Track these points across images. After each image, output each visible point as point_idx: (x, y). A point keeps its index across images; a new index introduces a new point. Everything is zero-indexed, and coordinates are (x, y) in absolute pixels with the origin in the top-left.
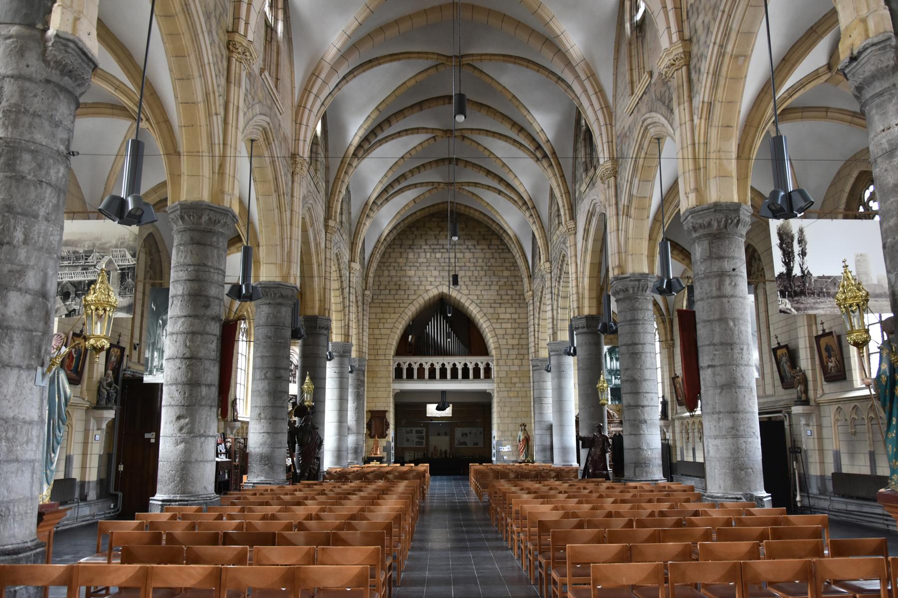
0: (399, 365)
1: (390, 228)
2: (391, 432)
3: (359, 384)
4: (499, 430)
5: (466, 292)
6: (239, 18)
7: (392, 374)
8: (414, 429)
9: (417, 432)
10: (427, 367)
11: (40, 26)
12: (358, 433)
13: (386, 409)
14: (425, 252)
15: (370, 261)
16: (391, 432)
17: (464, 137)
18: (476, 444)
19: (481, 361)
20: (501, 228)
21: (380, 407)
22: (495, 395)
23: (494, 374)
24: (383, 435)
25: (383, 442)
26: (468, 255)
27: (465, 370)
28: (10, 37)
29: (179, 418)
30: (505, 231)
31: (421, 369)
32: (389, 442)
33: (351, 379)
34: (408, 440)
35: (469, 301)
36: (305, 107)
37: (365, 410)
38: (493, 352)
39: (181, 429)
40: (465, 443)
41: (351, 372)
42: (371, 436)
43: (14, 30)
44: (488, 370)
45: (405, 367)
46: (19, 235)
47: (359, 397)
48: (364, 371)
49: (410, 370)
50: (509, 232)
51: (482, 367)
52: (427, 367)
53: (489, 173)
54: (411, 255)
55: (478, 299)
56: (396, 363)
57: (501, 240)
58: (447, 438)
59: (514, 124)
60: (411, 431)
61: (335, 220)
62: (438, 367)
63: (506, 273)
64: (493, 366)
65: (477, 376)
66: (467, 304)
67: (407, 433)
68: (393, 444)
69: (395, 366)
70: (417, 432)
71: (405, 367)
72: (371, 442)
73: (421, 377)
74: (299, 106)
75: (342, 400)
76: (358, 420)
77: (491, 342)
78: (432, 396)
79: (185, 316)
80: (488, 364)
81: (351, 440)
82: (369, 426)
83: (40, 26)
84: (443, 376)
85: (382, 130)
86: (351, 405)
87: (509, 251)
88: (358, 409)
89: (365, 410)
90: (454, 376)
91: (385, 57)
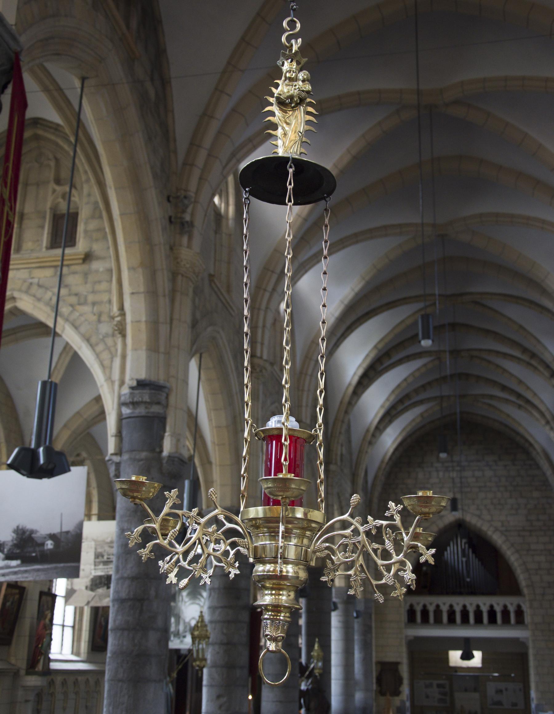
0: (411, 606)
1: (394, 446)
2: (405, 689)
3: (367, 631)
4: (537, 690)
5: (488, 517)
6: (212, 117)
7: (404, 617)
8: (435, 682)
9: (439, 686)
10: (445, 609)
11: (158, 450)
12: (367, 690)
13: (398, 660)
14: (437, 471)
15: (374, 485)
16: (405, 689)
17: (472, 357)
18: (515, 705)
19: (511, 602)
20: (527, 441)
21: (390, 657)
22: (530, 645)
23: (527, 619)
24: (397, 693)
25: (397, 701)
26: (489, 473)
27: (492, 613)
28: (142, 460)
29: (219, 697)
30: (531, 445)
31: (438, 611)
32: (403, 702)
33: (357, 626)
34: (427, 697)
35: (492, 529)
36: (306, 374)
37: (374, 660)
38: (525, 591)
39: (220, 707)
40: (499, 703)
41: (357, 617)
42: (381, 692)
43: (144, 455)
44: (519, 613)
45: (418, 609)
46: (152, 592)
47: (366, 646)
48: (371, 615)
49: (425, 613)
50: (536, 446)
51: (512, 609)
52: (445, 609)
53: (504, 388)
54: (421, 475)
55: (503, 526)
56: (408, 604)
57: (527, 453)
58: (476, 695)
59: (525, 350)
60: (431, 685)
61: (336, 464)
62: (458, 609)
63: (536, 494)
64: (525, 608)
65: (506, 620)
66: (490, 533)
67: (427, 686)
68: (408, 704)
69: (407, 607)
70: (439, 686)
71: (418, 609)
72: (382, 700)
73: (438, 621)
74: (301, 373)
75: (348, 652)
76: (367, 673)
77: (522, 579)
78: (455, 643)
79: (222, 607)
80: (519, 606)
81: (359, 696)
82: (379, 680)
83: (158, 450)
84: (465, 620)
85: (382, 364)
86: (357, 655)
87: (538, 467)
88: (366, 660)
89: (374, 660)
90: (479, 620)
91: (381, 307)
